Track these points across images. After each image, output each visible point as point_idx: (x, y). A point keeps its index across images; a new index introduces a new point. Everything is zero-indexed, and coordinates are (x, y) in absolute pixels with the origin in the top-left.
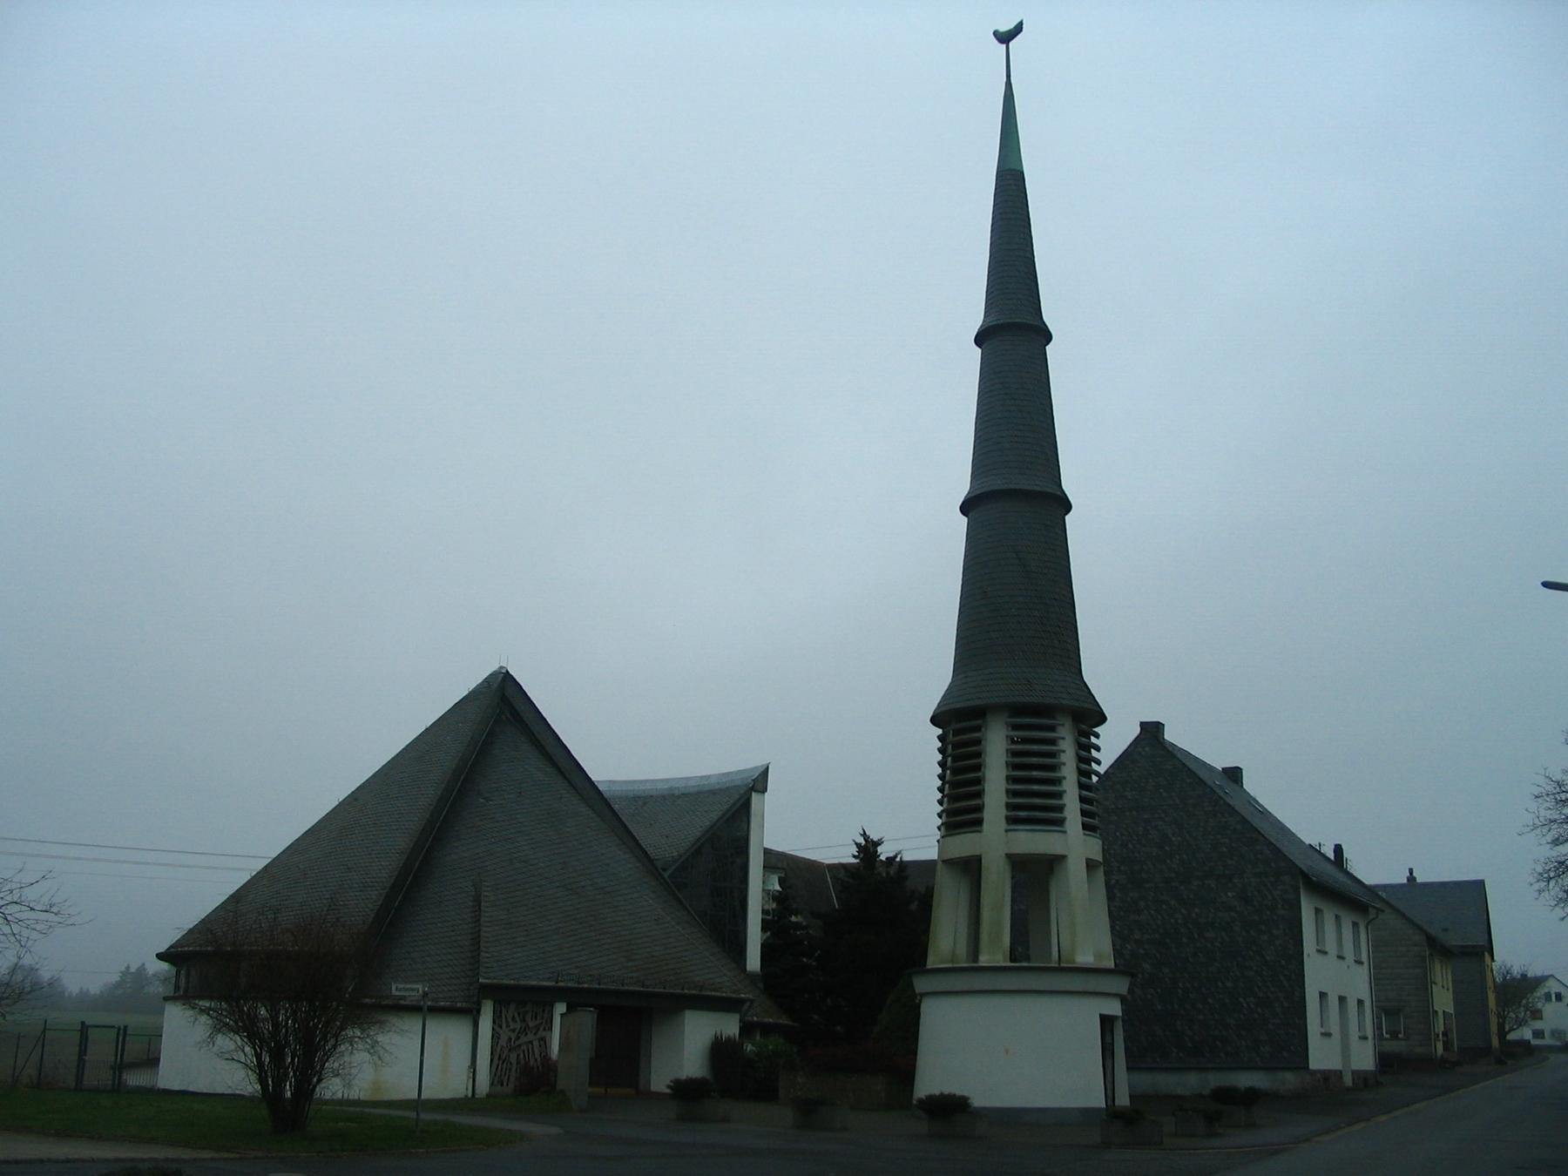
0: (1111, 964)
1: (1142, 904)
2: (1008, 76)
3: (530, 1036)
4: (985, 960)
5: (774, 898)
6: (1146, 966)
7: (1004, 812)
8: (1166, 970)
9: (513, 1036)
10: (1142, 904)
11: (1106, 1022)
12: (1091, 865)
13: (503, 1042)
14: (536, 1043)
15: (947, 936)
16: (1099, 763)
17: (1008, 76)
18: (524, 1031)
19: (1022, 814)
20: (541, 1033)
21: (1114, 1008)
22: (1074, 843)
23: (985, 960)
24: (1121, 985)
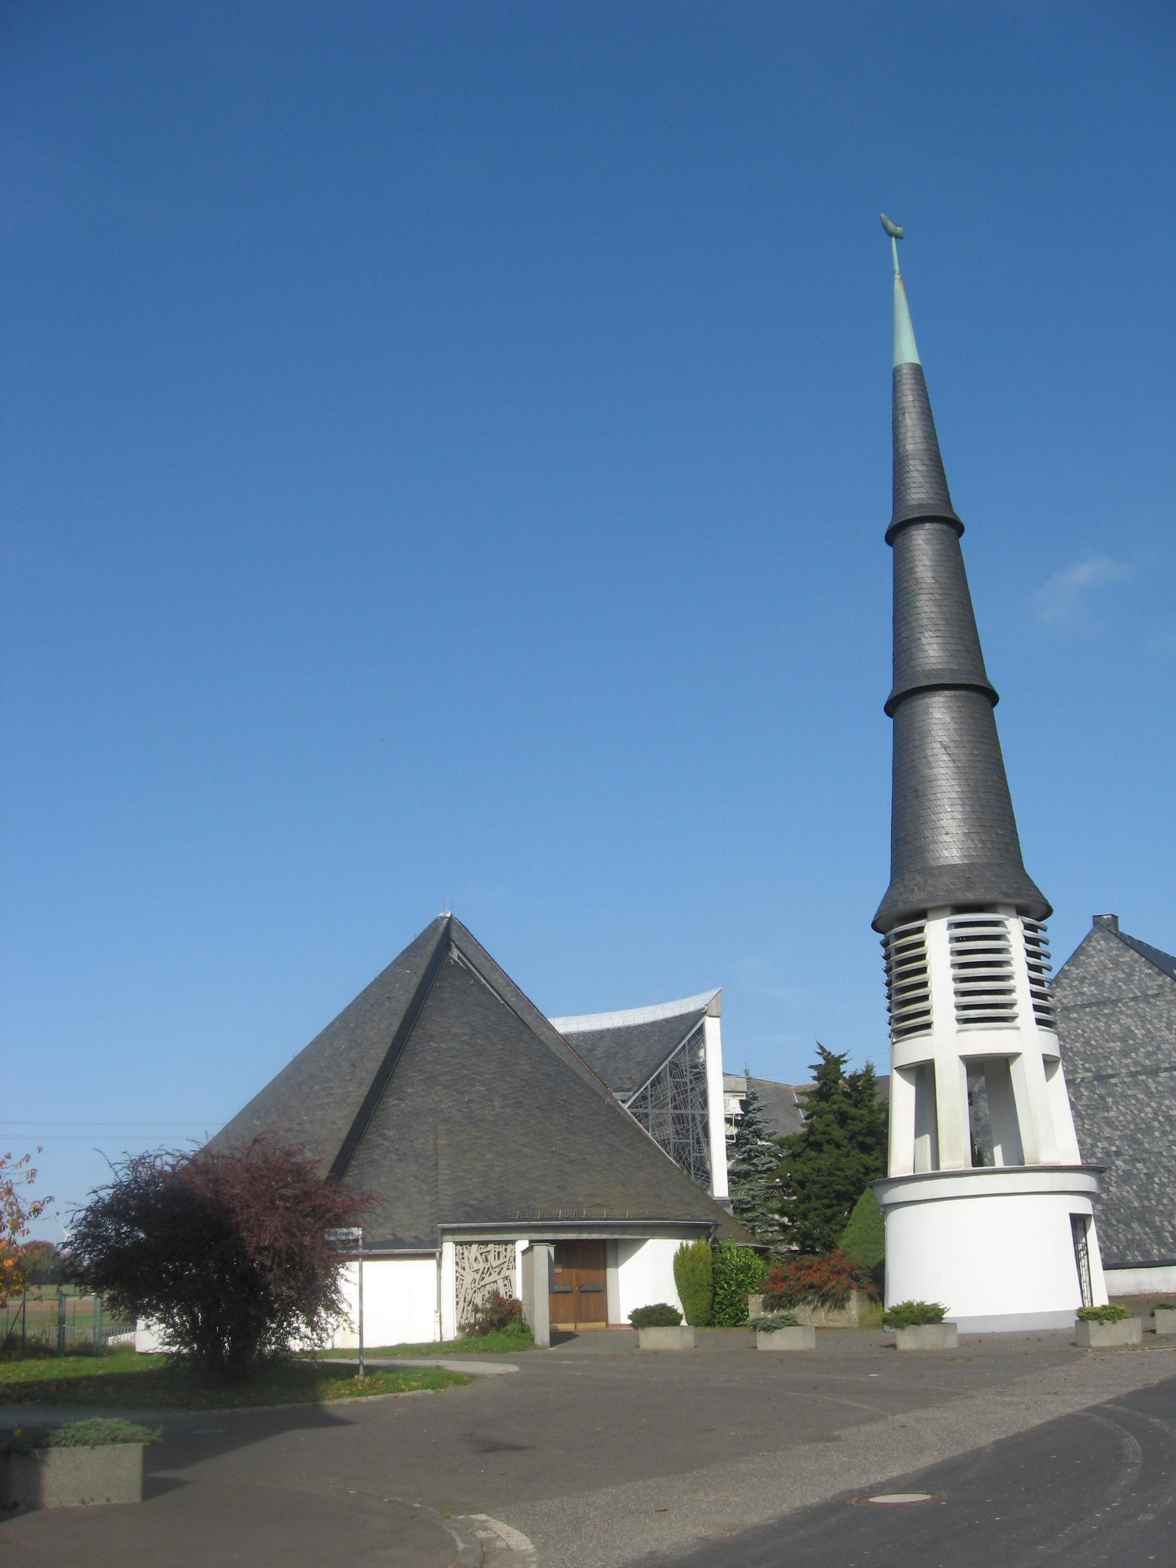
0: (1078, 1162)
1: (1110, 1100)
2: (439, 1278)
3: (495, 1276)
4: (945, 1166)
5: (738, 1124)
6: (1118, 1163)
7: (954, 999)
8: (1139, 1165)
9: (477, 1277)
10: (1110, 1100)
11: (1078, 1223)
12: (1049, 1063)
13: (467, 1283)
14: (500, 1282)
15: (904, 1150)
16: (1049, 969)
17: (439, 1278)
18: (487, 1271)
19: (909, 398)
20: (505, 1273)
21: (1084, 1206)
22: (1025, 1040)
23: (945, 1166)
24: (1087, 1182)
